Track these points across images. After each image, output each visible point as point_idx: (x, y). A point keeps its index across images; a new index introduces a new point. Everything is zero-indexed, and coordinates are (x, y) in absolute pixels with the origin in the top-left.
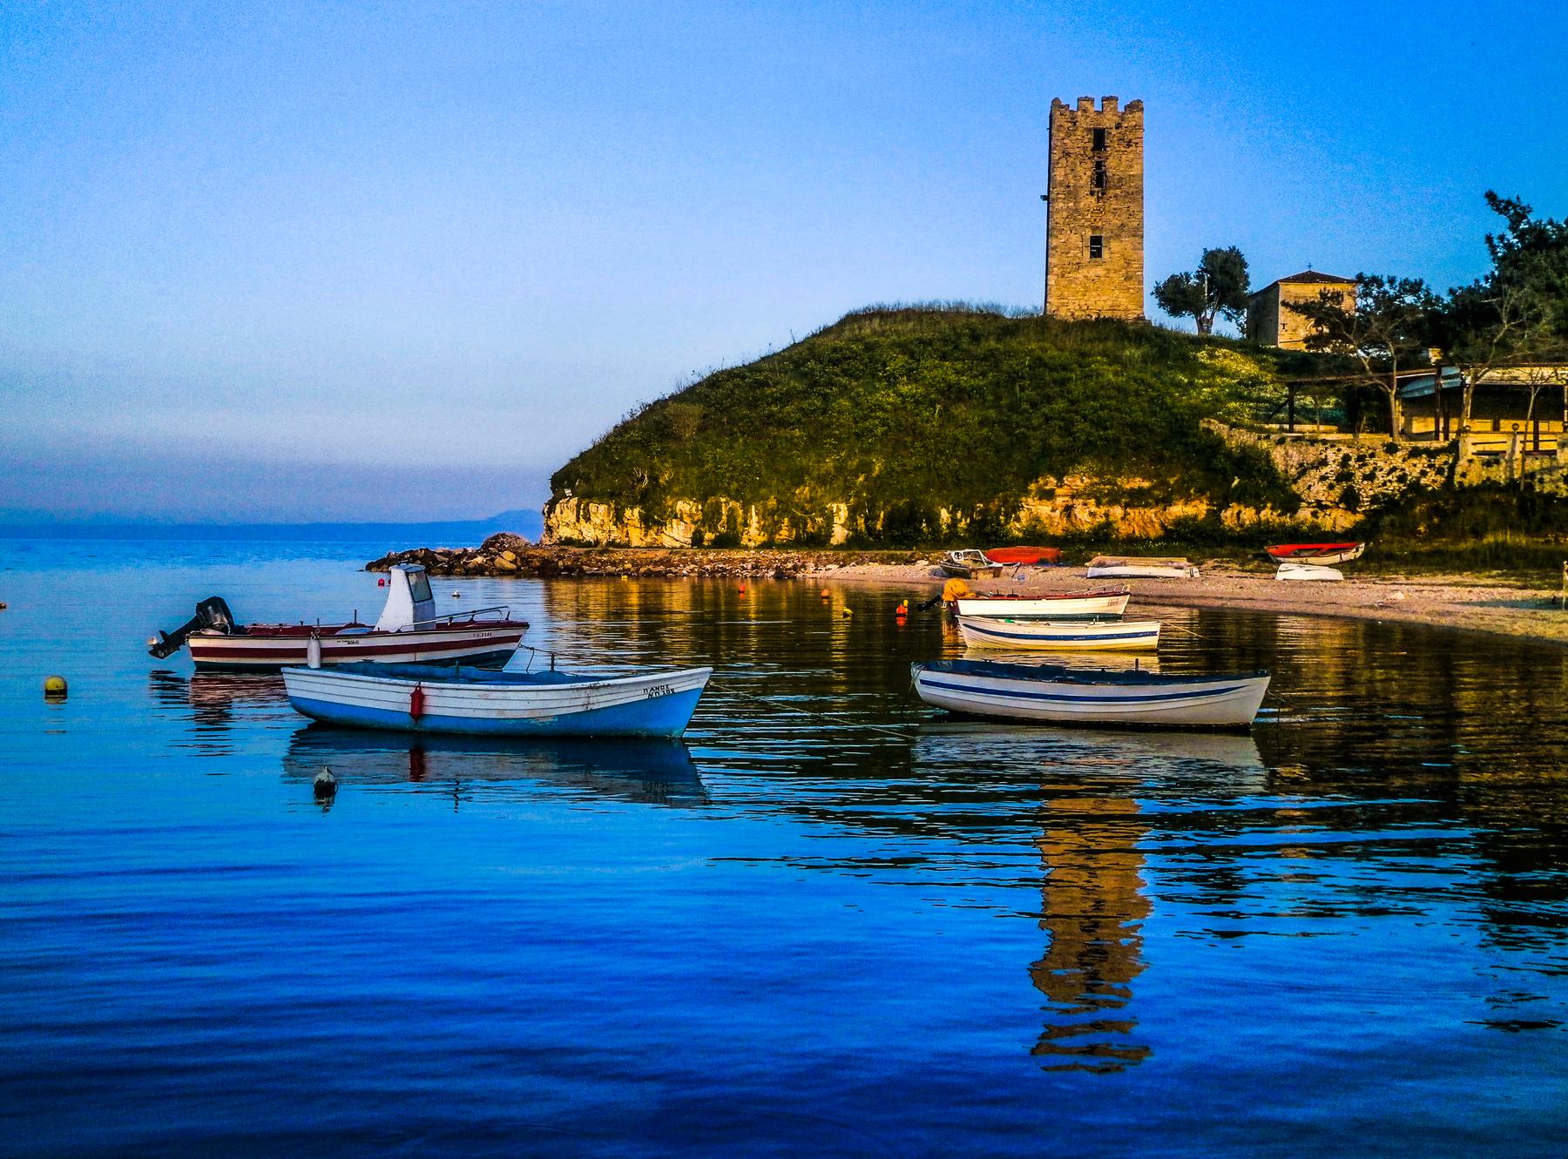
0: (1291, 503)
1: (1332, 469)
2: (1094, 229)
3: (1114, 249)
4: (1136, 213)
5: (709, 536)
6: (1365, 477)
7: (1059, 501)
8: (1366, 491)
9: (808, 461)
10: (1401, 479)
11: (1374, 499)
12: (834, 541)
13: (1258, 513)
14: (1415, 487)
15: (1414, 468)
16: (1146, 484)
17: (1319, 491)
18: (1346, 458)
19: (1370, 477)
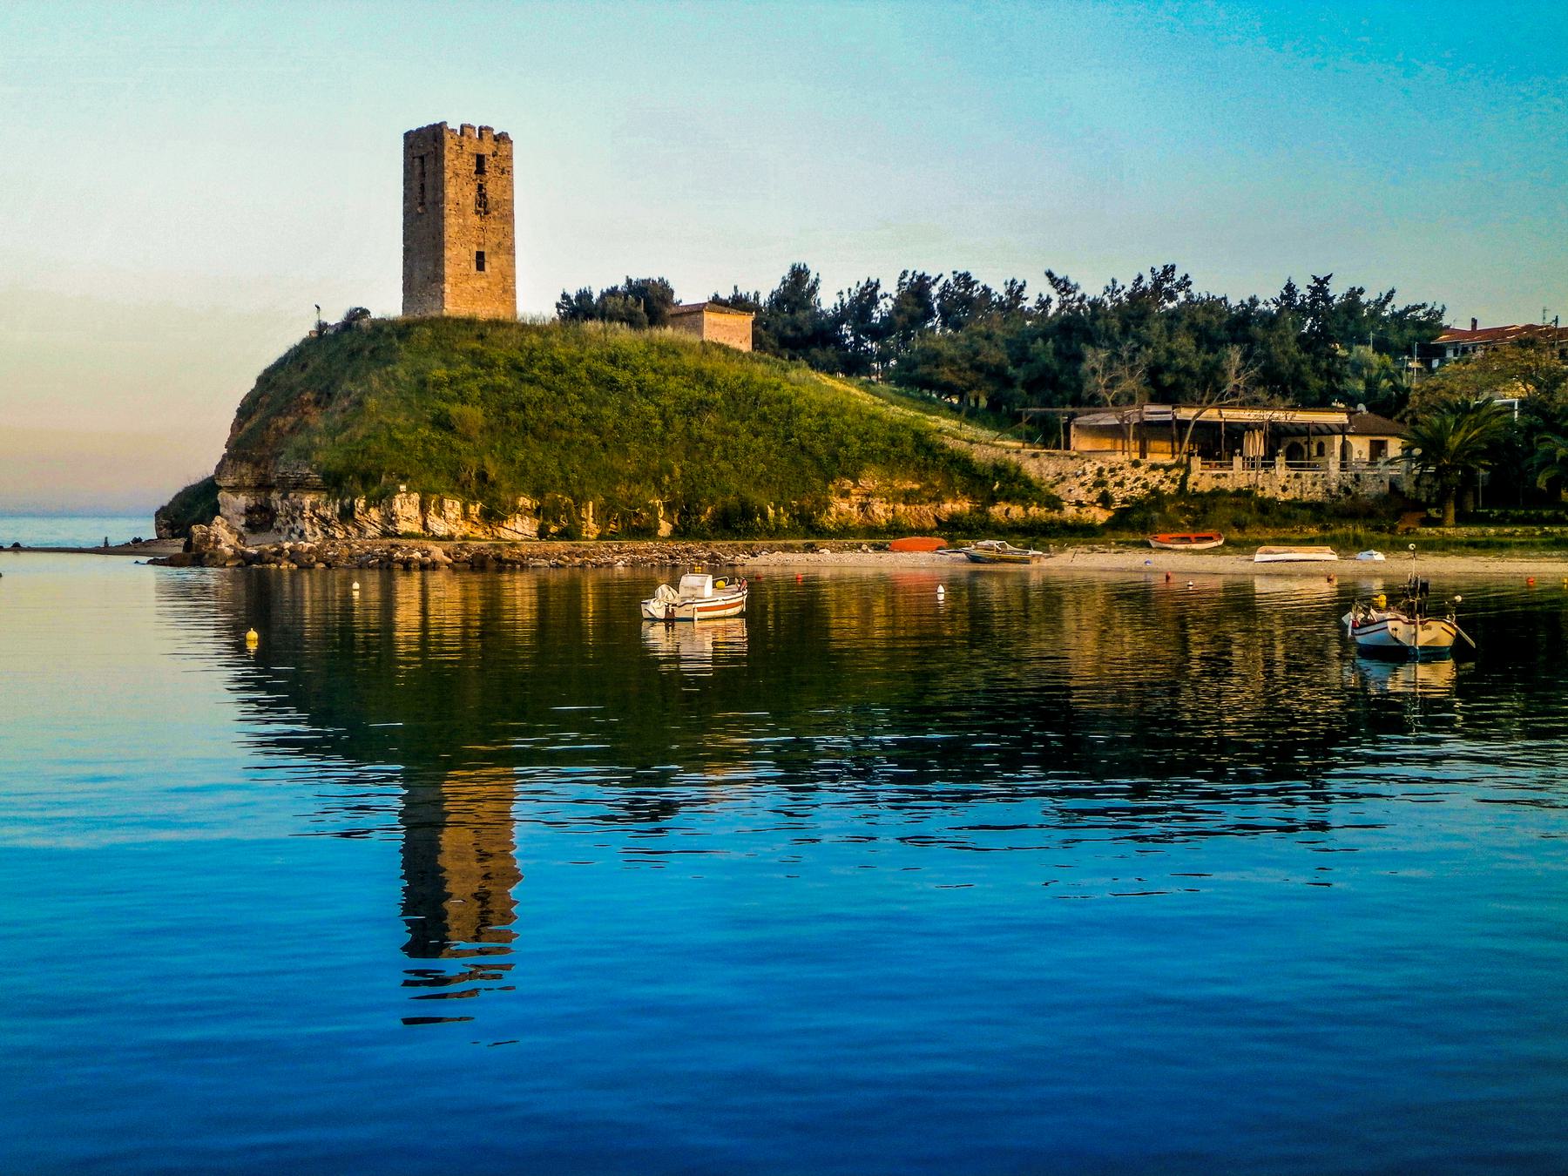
0: (1054, 503)
1: (1090, 477)
2: (479, 244)
3: (492, 264)
4: (509, 235)
5: (553, 529)
6: (1116, 484)
7: (853, 499)
8: (1118, 495)
9: (617, 462)
10: (1145, 486)
11: (1124, 501)
12: (660, 533)
13: (1026, 509)
14: (1154, 491)
15: (1154, 479)
16: (916, 486)
17: (1080, 493)
18: (1101, 470)
19: (1120, 484)
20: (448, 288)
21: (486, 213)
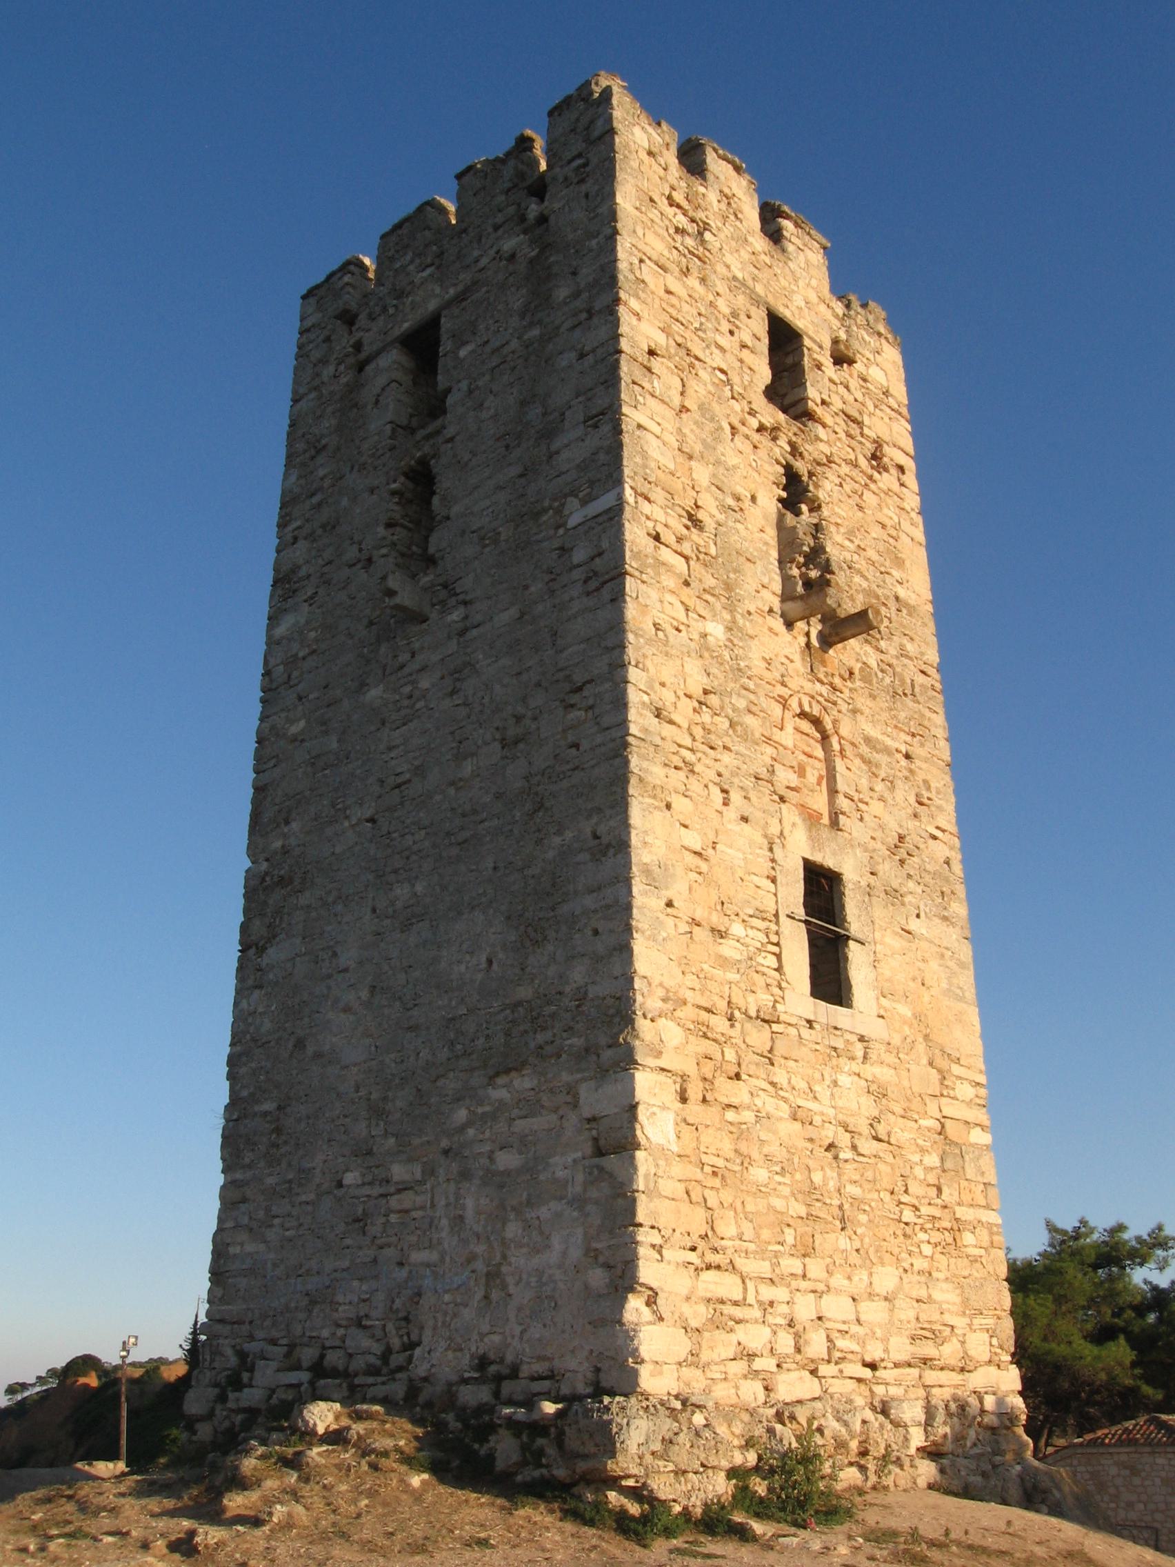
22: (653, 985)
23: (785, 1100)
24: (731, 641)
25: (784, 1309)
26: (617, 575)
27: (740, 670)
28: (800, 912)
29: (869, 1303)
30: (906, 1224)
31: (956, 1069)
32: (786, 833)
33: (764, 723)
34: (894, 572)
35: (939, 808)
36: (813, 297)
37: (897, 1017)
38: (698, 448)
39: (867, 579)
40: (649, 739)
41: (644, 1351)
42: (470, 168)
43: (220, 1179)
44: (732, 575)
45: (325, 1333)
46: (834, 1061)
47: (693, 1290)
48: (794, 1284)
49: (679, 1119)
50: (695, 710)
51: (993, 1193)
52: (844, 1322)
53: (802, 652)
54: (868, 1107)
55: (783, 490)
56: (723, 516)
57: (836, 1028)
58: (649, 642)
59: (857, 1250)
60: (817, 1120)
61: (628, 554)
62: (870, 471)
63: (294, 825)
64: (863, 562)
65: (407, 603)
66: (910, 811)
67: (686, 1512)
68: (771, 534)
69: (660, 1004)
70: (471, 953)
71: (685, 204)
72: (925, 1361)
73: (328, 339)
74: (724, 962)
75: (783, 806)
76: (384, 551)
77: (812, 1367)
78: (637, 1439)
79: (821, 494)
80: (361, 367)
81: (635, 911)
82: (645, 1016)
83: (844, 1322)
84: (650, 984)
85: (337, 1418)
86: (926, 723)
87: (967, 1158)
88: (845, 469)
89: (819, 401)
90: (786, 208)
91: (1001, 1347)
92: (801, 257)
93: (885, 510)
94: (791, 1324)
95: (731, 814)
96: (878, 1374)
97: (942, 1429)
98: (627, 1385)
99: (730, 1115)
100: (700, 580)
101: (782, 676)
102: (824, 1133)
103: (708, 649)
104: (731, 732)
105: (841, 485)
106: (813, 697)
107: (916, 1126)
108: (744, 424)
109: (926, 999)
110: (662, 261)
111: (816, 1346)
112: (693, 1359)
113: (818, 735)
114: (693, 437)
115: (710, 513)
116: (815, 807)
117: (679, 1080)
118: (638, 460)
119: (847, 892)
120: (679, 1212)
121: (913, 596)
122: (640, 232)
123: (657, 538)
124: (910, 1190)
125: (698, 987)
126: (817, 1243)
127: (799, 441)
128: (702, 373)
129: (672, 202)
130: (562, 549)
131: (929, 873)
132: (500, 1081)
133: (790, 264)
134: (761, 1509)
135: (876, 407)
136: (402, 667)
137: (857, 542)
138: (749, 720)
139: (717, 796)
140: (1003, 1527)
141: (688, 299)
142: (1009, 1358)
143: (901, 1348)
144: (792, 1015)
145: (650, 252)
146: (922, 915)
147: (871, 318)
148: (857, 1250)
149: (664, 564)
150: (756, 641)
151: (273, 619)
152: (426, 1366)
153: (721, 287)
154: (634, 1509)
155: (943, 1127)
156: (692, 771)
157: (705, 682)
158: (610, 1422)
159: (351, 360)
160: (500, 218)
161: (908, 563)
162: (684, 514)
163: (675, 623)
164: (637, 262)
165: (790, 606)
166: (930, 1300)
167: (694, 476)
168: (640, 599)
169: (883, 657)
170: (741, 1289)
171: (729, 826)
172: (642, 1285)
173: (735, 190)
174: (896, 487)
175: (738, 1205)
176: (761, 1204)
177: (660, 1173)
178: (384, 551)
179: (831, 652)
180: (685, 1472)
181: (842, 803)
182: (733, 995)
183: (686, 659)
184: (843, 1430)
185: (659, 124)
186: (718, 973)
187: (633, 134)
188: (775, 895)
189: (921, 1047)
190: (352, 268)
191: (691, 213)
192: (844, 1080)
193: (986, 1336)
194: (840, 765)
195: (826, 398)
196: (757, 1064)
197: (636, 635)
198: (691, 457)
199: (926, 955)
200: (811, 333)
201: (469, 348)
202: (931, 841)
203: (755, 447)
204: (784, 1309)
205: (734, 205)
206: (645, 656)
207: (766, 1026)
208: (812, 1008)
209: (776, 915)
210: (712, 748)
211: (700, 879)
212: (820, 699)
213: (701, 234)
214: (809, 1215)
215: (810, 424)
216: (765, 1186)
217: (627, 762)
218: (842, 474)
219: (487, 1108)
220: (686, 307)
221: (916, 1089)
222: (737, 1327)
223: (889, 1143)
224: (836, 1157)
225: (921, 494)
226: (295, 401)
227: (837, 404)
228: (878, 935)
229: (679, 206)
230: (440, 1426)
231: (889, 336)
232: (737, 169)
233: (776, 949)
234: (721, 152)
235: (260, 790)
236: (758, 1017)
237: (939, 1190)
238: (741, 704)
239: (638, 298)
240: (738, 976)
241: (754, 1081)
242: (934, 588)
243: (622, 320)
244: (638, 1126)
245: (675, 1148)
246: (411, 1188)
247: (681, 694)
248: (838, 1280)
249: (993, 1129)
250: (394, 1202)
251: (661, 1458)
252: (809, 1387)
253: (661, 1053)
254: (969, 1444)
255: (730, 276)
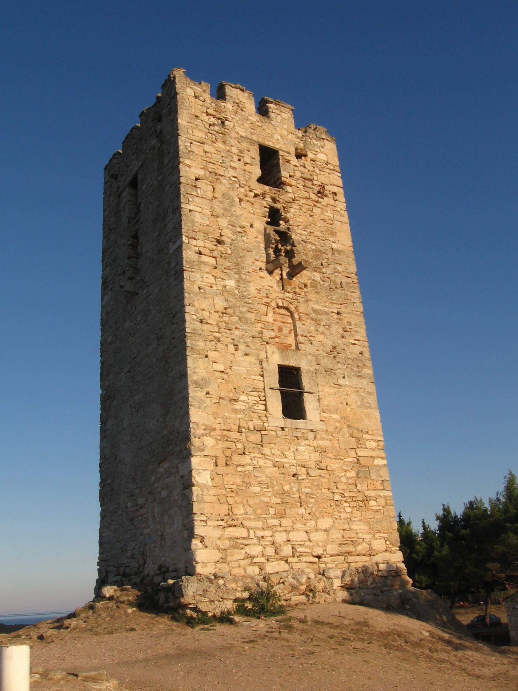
2: (284, 348)
20: (202, 472)
21: (295, 270)
22: (200, 425)
23: (270, 460)
24: (239, 286)
25: (270, 539)
26: (182, 271)
27: (243, 296)
28: (277, 386)
29: (315, 533)
30: (337, 501)
31: (365, 436)
32: (269, 356)
33: (257, 315)
34: (330, 239)
35: (357, 332)
36: (285, 133)
37: (331, 420)
38: (221, 212)
39: (315, 245)
40: (196, 332)
41: (198, 559)
42: (143, 113)
43: (100, 509)
44: (239, 259)
45: (125, 562)
46: (296, 442)
47: (222, 536)
48: (275, 529)
49: (213, 473)
50: (220, 317)
51: (387, 485)
52: (302, 541)
53: (278, 282)
54: (315, 457)
55: (269, 218)
56: (235, 237)
57: (297, 429)
58: (196, 295)
59: (309, 513)
60: (287, 465)
61: (184, 263)
62: (317, 199)
63: (111, 376)
64: (313, 238)
65: (128, 289)
66: (339, 335)
67: (214, 616)
68: (261, 238)
69: (203, 431)
70: (153, 419)
71: (214, 113)
72: (349, 553)
73: (111, 186)
74: (236, 411)
75: (267, 346)
76: (128, 268)
77: (285, 559)
78: (191, 591)
79: (288, 215)
80: (119, 196)
81: (190, 399)
82: (195, 437)
83: (302, 541)
84: (198, 425)
85: (115, 591)
86: (349, 298)
87: (372, 471)
88: (303, 201)
89: (288, 176)
90: (269, 99)
91: (392, 544)
92: (279, 118)
93: (326, 214)
94: (273, 544)
95: (240, 353)
96: (321, 560)
97: (348, 579)
98: (190, 571)
99: (240, 469)
100: (222, 265)
101: (267, 294)
102: (290, 470)
103: (226, 291)
104: (239, 322)
105: (300, 209)
106: (284, 299)
107: (343, 462)
108: (246, 196)
109: (349, 410)
110: (202, 140)
111: (287, 550)
112: (223, 560)
113: (289, 314)
114: (218, 208)
115: (228, 235)
116: (288, 343)
117: (214, 458)
118: (190, 224)
119: (302, 374)
120: (214, 507)
121: (342, 246)
122: (190, 132)
123: (200, 253)
124: (338, 487)
125: (222, 422)
126: (287, 512)
127: (277, 196)
128: (223, 181)
129: (207, 114)
130: (168, 263)
131: (350, 359)
132: (161, 465)
133: (272, 122)
134: (246, 613)
135: (320, 170)
136: (133, 313)
137: (309, 231)
138: (249, 315)
139: (232, 348)
140: (338, 614)
141: (216, 152)
142: (398, 549)
143: (332, 548)
144: (272, 427)
145: (195, 138)
146: (346, 377)
147: (318, 133)
148: (309, 513)
149: (203, 263)
150: (252, 283)
151: (102, 298)
152: (147, 570)
153: (233, 142)
154: (194, 615)
155: (358, 460)
156: (219, 341)
157: (225, 304)
158: (182, 585)
159: (117, 194)
160: (150, 133)
161: (338, 233)
162: (215, 240)
163: (210, 285)
164: (189, 144)
165: (269, 265)
166: (350, 529)
167: (219, 224)
168: (191, 279)
169: (324, 275)
170: (247, 533)
171: (238, 359)
172: (197, 535)
173: (241, 99)
174: (332, 202)
175: (245, 502)
176: (257, 501)
177: (204, 494)
178: (128, 268)
179: (294, 279)
180: (213, 601)
181: (300, 339)
182: (241, 423)
183: (215, 297)
184: (295, 582)
185: (200, 84)
186: (233, 416)
187: (186, 92)
188: (263, 381)
189: (345, 429)
190: (116, 156)
191: (218, 116)
192: (300, 448)
193: (383, 541)
194: (298, 324)
195: (292, 174)
196: (254, 448)
197: (189, 293)
198: (217, 217)
199: (349, 393)
200: (283, 149)
201: (145, 186)
202: (351, 346)
203: (252, 204)
204: (270, 539)
205: (241, 106)
206: (194, 301)
207: (259, 433)
208: (283, 423)
209: (264, 389)
210: (229, 330)
211: (224, 381)
212: (288, 299)
213: (223, 123)
214: (283, 503)
215: (284, 187)
216: (259, 493)
217: (186, 343)
218: (300, 204)
219: (159, 475)
220: (214, 156)
221: (342, 446)
222: (246, 547)
223: (327, 470)
224: (297, 479)
225: (347, 202)
226: (104, 211)
227: (298, 174)
228: (320, 389)
229: (211, 115)
230: (146, 591)
231: (328, 138)
232: (242, 90)
233: (264, 402)
234: (233, 85)
235: (102, 363)
236: (255, 430)
237: (356, 486)
238: (245, 309)
239: (189, 159)
240: (243, 416)
241: (252, 454)
242: (354, 241)
243: (181, 170)
244: (193, 478)
245: (211, 484)
246: (142, 507)
247: (212, 311)
248: (298, 526)
249: (387, 458)
250: (139, 513)
251: (203, 596)
252: (283, 566)
253: (204, 449)
254: (369, 583)
255: (239, 136)
